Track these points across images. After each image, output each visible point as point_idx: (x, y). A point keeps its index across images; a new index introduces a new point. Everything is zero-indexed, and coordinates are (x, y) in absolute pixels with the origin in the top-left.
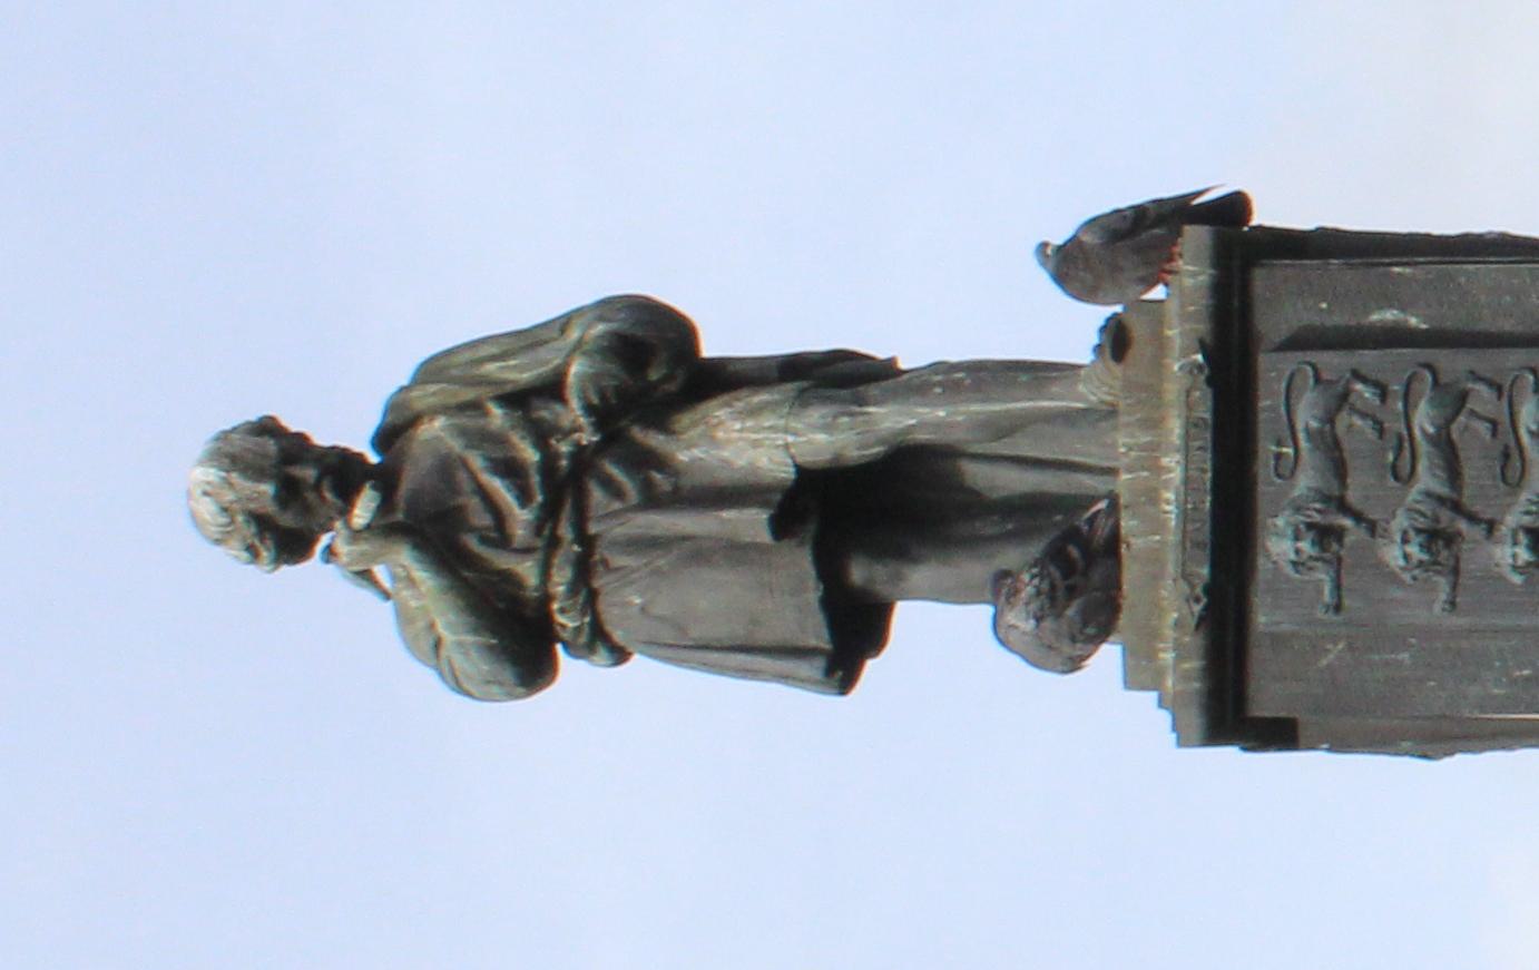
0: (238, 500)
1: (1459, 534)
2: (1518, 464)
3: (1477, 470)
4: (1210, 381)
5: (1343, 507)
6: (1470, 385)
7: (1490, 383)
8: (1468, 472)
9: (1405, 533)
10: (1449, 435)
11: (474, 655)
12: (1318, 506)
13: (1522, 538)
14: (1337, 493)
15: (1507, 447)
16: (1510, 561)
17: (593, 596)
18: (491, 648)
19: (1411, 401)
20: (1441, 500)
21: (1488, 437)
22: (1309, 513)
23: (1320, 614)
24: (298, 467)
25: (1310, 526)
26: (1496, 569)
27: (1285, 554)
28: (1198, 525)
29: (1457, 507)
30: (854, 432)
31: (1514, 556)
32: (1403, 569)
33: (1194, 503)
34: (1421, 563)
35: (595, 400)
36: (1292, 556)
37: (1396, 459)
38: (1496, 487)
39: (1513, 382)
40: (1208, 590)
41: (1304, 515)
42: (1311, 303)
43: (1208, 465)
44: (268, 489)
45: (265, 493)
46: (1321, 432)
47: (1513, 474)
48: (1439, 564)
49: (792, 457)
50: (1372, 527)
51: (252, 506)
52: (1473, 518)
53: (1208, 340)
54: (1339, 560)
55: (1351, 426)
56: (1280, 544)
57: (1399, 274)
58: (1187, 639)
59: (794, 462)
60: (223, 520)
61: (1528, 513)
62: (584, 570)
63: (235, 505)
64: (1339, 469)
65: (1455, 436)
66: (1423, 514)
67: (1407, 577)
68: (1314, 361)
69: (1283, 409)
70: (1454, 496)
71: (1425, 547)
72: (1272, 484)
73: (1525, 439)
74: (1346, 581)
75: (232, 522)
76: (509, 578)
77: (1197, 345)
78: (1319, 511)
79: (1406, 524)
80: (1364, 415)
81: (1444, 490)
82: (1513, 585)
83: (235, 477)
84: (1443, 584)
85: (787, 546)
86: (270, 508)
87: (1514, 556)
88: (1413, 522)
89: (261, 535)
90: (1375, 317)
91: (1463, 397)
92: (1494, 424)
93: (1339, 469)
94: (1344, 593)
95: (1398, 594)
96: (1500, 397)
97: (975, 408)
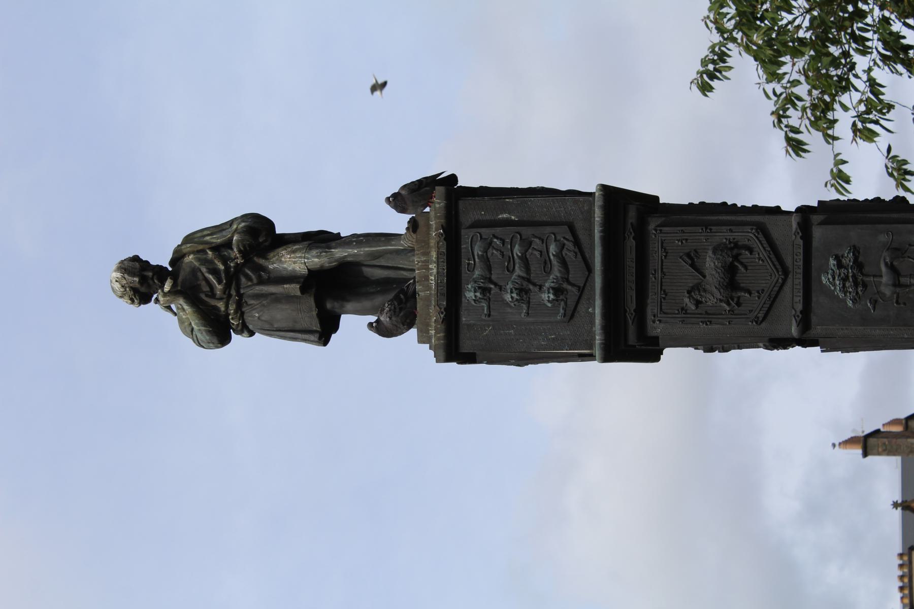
0: (127, 283)
1: (530, 290)
7: (540, 238)
8: (532, 269)
9: (549, 289)
10: (526, 255)
13: (551, 291)
15: (545, 260)
16: (547, 299)
17: (242, 314)
18: (209, 331)
20: (523, 278)
21: (539, 257)
28: (442, 288)
29: (529, 281)
31: (549, 297)
34: (517, 300)
36: (474, 298)
39: (547, 237)
44: (137, 279)
46: (482, 256)
47: (548, 270)
48: (523, 300)
49: (306, 267)
50: (501, 288)
51: (131, 285)
52: (534, 285)
53: (444, 225)
54: (489, 299)
55: (493, 253)
56: (470, 295)
60: (122, 290)
61: (553, 282)
62: (239, 305)
64: (489, 268)
65: (528, 257)
66: (517, 283)
67: (512, 304)
70: (528, 277)
71: (554, 294)
73: (552, 257)
75: (126, 290)
77: (441, 227)
78: (482, 282)
83: (126, 276)
86: (137, 285)
87: (549, 297)
91: (530, 243)
92: (541, 252)
93: (489, 268)
94: (491, 310)
95: (509, 310)
96: (543, 243)
97: (367, 249)
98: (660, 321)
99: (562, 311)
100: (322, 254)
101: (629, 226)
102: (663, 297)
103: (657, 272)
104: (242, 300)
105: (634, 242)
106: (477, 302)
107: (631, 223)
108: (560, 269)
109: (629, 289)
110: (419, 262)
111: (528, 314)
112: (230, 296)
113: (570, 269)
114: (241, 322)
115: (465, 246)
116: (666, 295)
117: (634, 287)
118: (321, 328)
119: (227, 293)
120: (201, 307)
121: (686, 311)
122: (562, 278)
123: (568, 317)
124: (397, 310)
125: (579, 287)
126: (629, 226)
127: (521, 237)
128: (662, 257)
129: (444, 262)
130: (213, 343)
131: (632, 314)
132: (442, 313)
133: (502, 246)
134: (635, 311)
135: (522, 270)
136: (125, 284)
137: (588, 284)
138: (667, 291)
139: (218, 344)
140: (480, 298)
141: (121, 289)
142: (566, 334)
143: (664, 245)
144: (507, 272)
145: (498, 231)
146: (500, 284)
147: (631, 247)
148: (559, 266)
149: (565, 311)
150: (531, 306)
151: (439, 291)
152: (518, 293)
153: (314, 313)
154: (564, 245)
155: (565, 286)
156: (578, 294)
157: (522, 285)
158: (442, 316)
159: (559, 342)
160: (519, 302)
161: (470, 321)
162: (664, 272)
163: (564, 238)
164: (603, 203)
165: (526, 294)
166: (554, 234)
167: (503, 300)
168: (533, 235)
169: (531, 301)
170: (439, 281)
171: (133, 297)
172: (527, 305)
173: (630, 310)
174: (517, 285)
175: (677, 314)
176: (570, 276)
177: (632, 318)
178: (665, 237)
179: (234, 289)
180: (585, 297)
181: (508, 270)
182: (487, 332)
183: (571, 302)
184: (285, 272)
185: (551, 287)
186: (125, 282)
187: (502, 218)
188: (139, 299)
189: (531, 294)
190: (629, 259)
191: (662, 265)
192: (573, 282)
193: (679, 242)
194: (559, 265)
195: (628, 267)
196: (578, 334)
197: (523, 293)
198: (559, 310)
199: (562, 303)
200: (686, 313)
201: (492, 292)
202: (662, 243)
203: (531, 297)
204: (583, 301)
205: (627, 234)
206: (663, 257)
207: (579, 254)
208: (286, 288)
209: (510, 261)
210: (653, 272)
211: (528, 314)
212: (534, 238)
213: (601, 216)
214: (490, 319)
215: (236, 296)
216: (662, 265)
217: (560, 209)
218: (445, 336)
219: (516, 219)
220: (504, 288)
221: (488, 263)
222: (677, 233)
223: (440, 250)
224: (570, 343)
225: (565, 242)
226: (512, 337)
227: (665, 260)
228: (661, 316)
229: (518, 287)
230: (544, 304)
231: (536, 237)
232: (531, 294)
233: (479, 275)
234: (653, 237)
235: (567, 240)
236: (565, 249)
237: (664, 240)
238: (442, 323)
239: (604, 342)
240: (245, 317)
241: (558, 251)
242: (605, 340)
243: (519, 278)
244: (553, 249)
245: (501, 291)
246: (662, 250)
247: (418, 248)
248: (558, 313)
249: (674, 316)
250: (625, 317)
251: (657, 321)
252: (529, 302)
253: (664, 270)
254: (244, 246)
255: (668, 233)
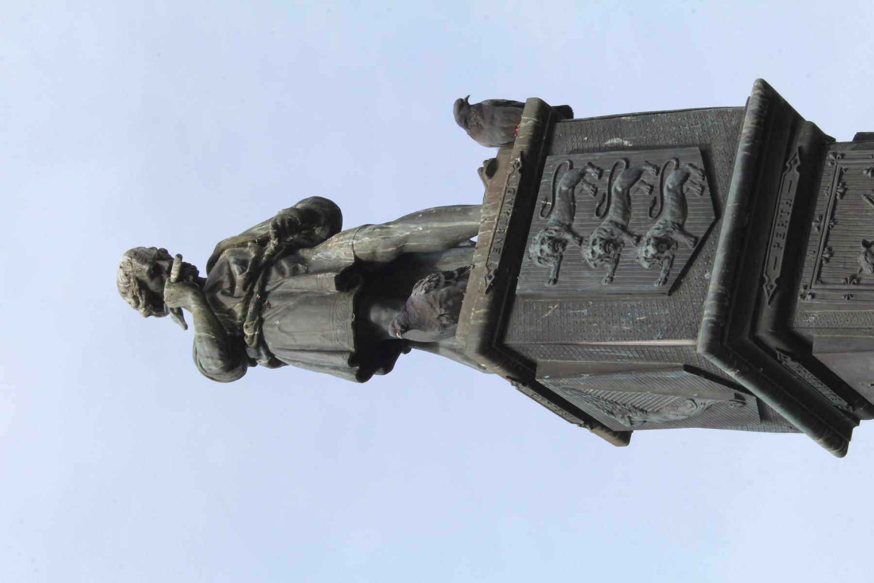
0: (133, 271)
1: (623, 242)
2: (660, 206)
3: (638, 210)
4: (521, 171)
5: (569, 229)
6: (644, 168)
7: (654, 166)
8: (634, 211)
10: (628, 192)
11: (204, 343)
12: (557, 228)
14: (567, 223)
15: (655, 198)
16: (644, 255)
17: (261, 321)
18: (211, 340)
19: (613, 178)
20: (616, 224)
21: (647, 194)
22: (550, 231)
23: (546, 285)
24: (162, 261)
25: (550, 238)
26: (637, 261)
27: (536, 253)
28: (498, 240)
29: (624, 229)
30: (381, 237)
32: (590, 260)
33: (500, 229)
34: (600, 256)
35: (279, 223)
36: (539, 254)
37: (600, 206)
38: (646, 219)
39: (666, 165)
40: (496, 273)
41: (549, 232)
42: (580, 137)
43: (510, 212)
44: (146, 267)
45: (145, 269)
46: (566, 192)
48: (609, 257)
49: (354, 252)
50: (581, 241)
51: (138, 275)
52: (631, 234)
53: (525, 151)
54: (561, 257)
55: (582, 190)
56: (535, 249)
57: (624, 119)
58: (482, 298)
59: (354, 254)
60: (125, 280)
62: (260, 307)
63: (131, 274)
64: (572, 211)
65: (631, 194)
66: (605, 231)
67: (592, 265)
68: (571, 159)
69: (552, 184)
70: (624, 223)
72: (539, 220)
73: (665, 193)
74: (562, 267)
75: (129, 282)
76: (231, 313)
77: (519, 153)
78: (556, 231)
79: (596, 237)
80: (589, 184)
81: (619, 220)
82: (644, 269)
83: (134, 261)
84: (609, 267)
85: (343, 295)
86: (146, 278)
87: (647, 251)
88: (599, 234)
89: (140, 290)
90: (609, 142)
91: (640, 173)
92: (652, 187)
93: (572, 211)
94: (560, 274)
95: (586, 273)
96: (657, 173)
97: (436, 225)
98: (813, 296)
99: (663, 275)
100: (375, 231)
101: (796, 150)
102: (826, 258)
103: (823, 220)
104: (265, 301)
105: (797, 174)
106: (542, 261)
107: (800, 149)
108: (674, 209)
109: (775, 246)
110: (486, 220)
111: (612, 279)
112: (251, 293)
113: (689, 212)
114: (256, 333)
115: (545, 180)
116: (831, 255)
117: (783, 243)
118: (355, 347)
119: (248, 289)
120: (216, 314)
121: (859, 280)
122: (673, 223)
123: (669, 285)
124: (442, 284)
125: (696, 239)
126: (796, 150)
127: (627, 166)
128: (836, 195)
129: (511, 204)
130: (212, 358)
131: (772, 287)
132: (490, 277)
133: (597, 178)
134: (777, 281)
135: (617, 212)
136: (130, 272)
137: (711, 236)
138: (834, 249)
139: (219, 359)
140: (548, 255)
141: (123, 279)
142: (663, 313)
143: (844, 177)
144: (596, 218)
145: (597, 158)
146: (581, 235)
147: (791, 182)
148: (673, 205)
149: (668, 275)
150: (618, 267)
151: (494, 245)
152: (603, 245)
153: (350, 321)
154: (688, 175)
155: (677, 236)
156: (693, 249)
157: (612, 235)
158: (489, 282)
159: (650, 326)
160: (602, 261)
161: (525, 290)
162: (834, 220)
163: (691, 165)
164: (757, 107)
165: (615, 247)
166: (677, 160)
167: (581, 258)
168: (646, 162)
169: (621, 260)
170: (497, 231)
171: (138, 295)
172: (614, 265)
173: (769, 280)
174: (604, 233)
175: (844, 284)
176: (687, 221)
177: (771, 292)
178: (846, 164)
179: (259, 285)
180: (703, 255)
181: (598, 214)
182: (550, 312)
183: (680, 263)
184: (328, 262)
185: (653, 237)
186: (130, 269)
187: (611, 144)
188: (146, 299)
189: (623, 249)
190: (784, 199)
191: (834, 209)
192: (690, 232)
193: (868, 172)
194: (674, 203)
195: (780, 212)
196: (681, 314)
197: (611, 245)
198: (659, 275)
199: (666, 262)
200: (858, 283)
201: (568, 246)
202: (841, 174)
203: (622, 254)
204: (699, 262)
205: (790, 163)
206: (839, 194)
207: (707, 192)
208: (319, 278)
209: (603, 200)
210: (818, 219)
211: (612, 279)
212: (646, 165)
213: (751, 126)
214: (555, 286)
215: (257, 293)
216: (834, 209)
217: (695, 126)
218: (486, 314)
219: (630, 145)
220: (586, 241)
221: (572, 203)
222: (867, 158)
223: (510, 186)
224: (665, 328)
225: (691, 170)
226: (584, 319)
227: (840, 201)
228: (818, 286)
229: (605, 237)
230: (639, 265)
231: (650, 165)
232: (623, 249)
233: (554, 220)
234: (829, 164)
235: (695, 167)
236: (688, 181)
237: (846, 170)
238: (487, 292)
239: (714, 319)
240: (264, 328)
241: (676, 183)
242: (717, 317)
243: (610, 224)
244: (670, 180)
245: (580, 245)
246: (838, 185)
247: (491, 198)
248: (656, 279)
249: (837, 287)
250: (761, 290)
251: (808, 295)
252: (617, 262)
253: (836, 216)
254: (283, 221)
255: (853, 159)
